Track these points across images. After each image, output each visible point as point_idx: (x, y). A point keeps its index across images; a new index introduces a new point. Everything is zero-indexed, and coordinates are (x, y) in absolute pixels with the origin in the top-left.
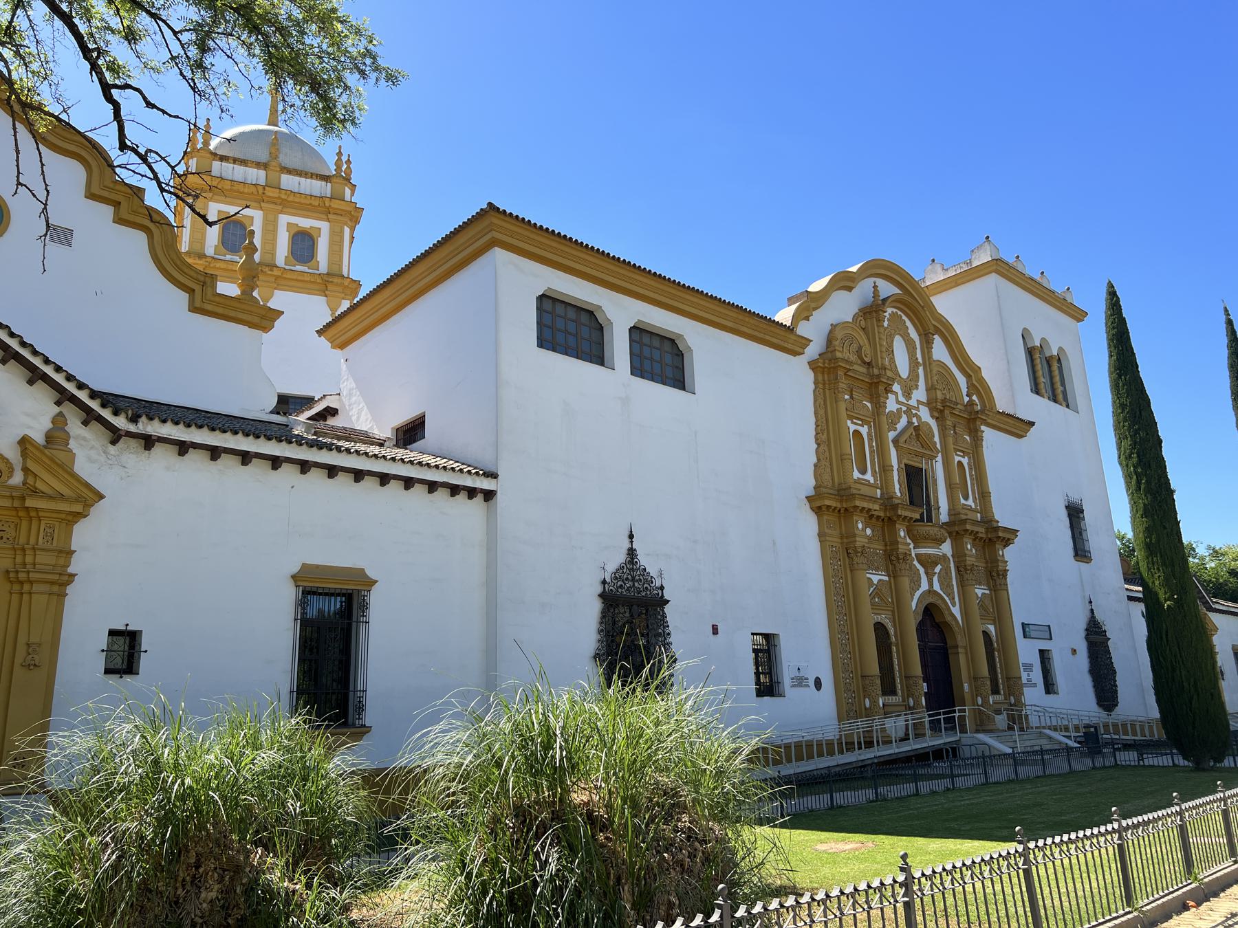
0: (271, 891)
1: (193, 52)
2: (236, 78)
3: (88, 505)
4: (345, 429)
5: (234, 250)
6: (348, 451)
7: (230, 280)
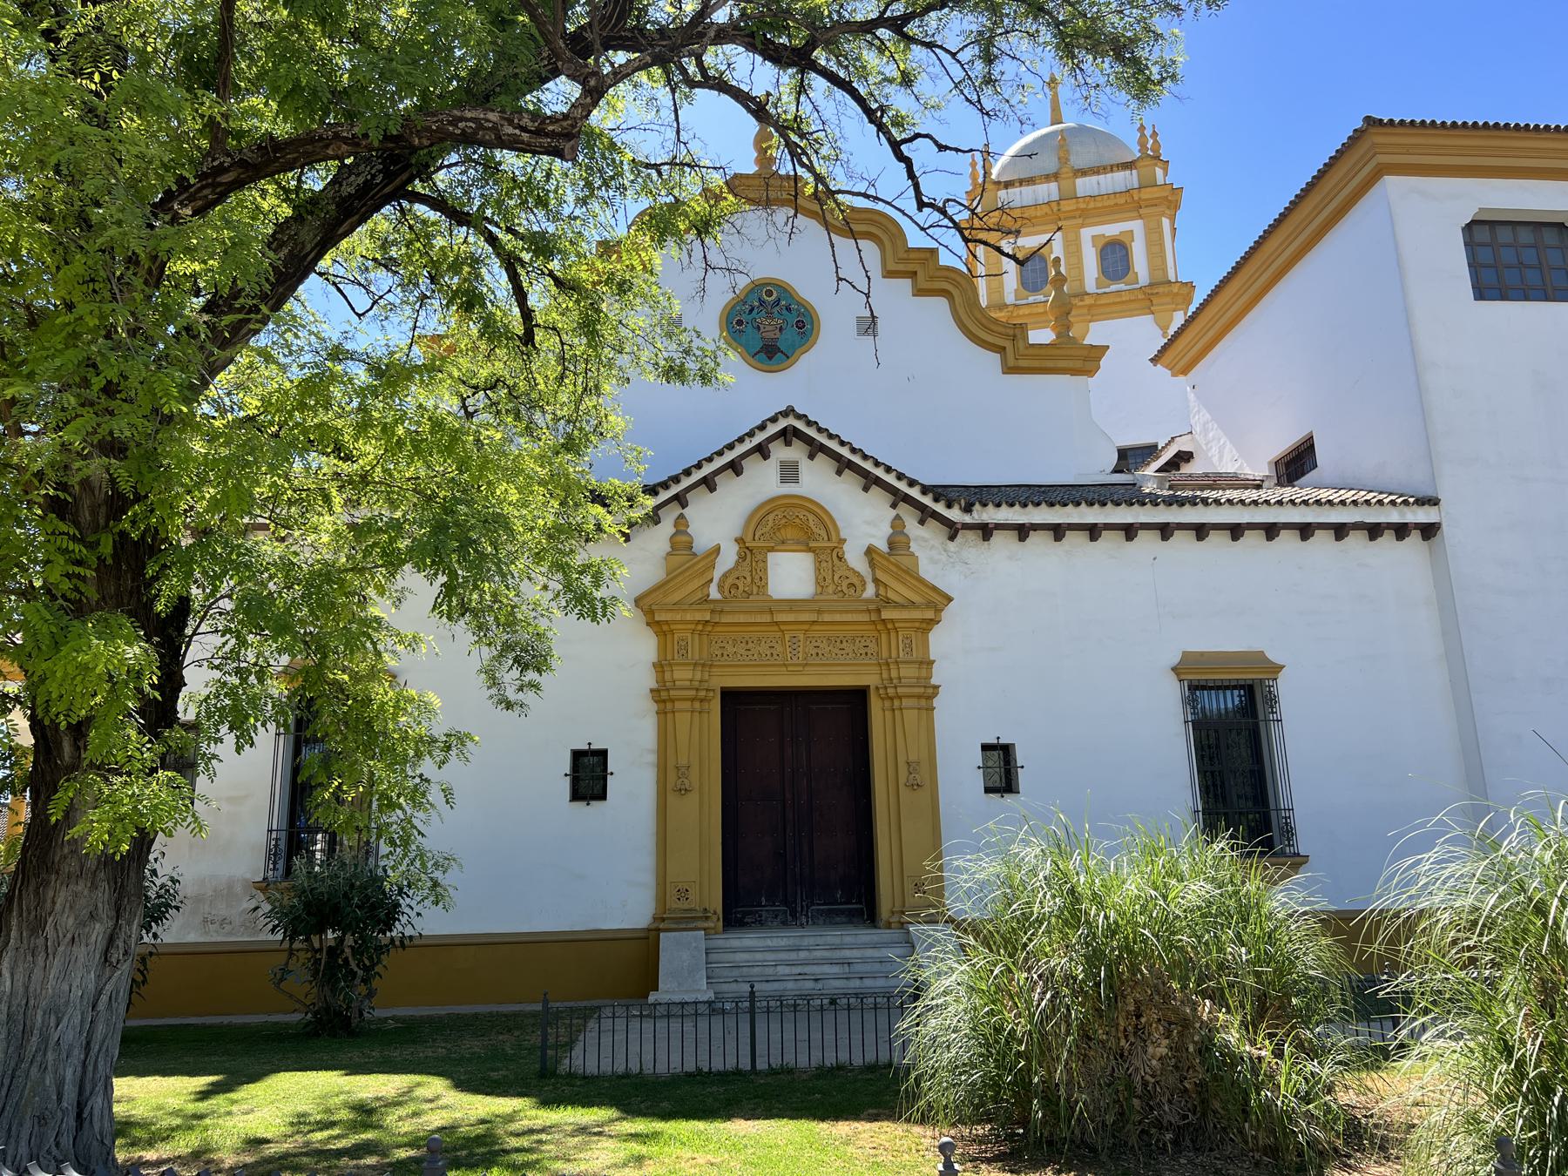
0: (1232, 1055)
1: (979, 66)
2: (1028, 79)
3: (938, 611)
4: (1207, 475)
5: (1035, 289)
6: (1217, 502)
7: (1041, 325)
